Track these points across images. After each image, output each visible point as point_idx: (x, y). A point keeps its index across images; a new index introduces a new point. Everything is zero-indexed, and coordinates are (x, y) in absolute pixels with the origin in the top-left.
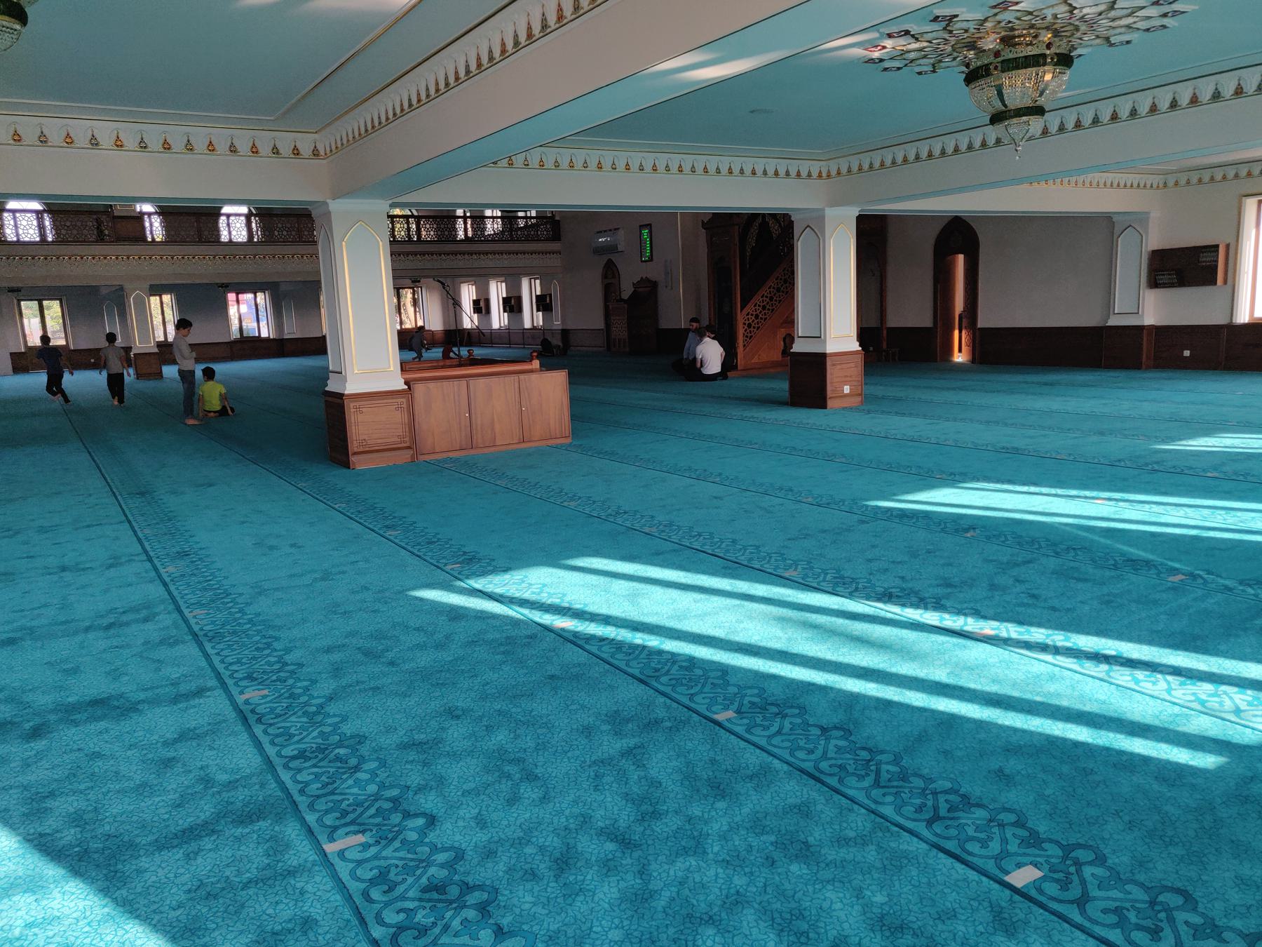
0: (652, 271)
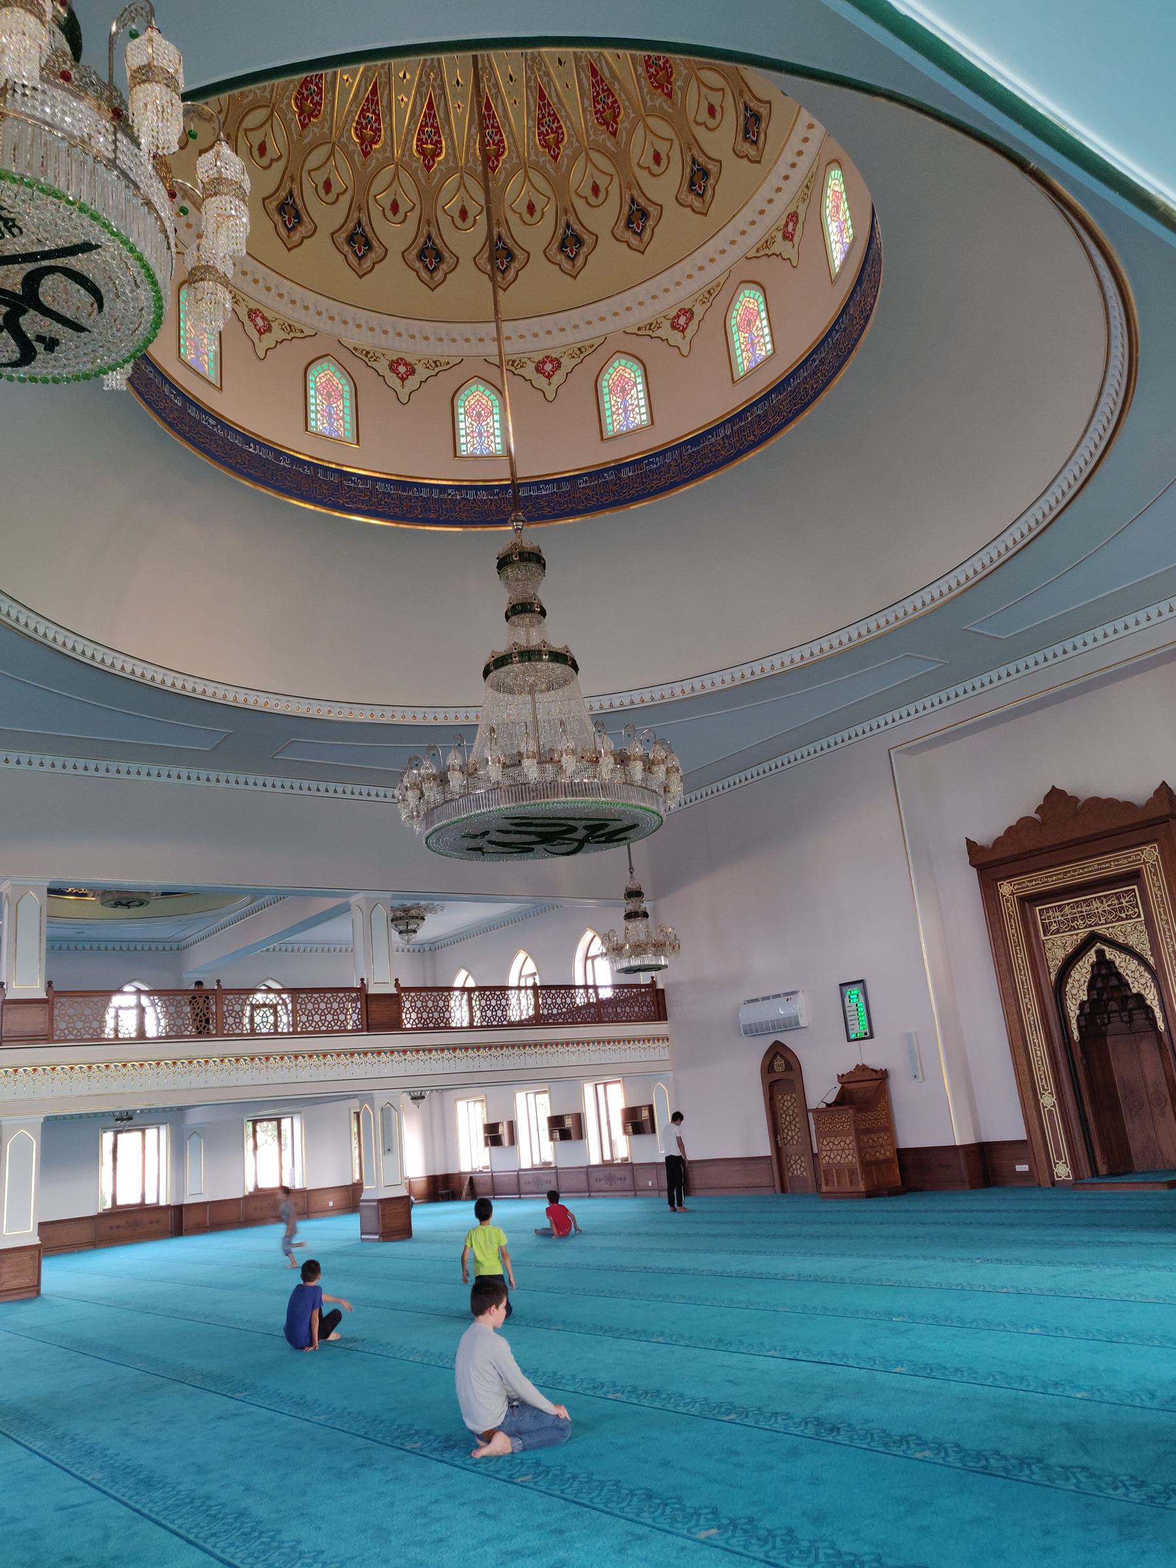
0: (873, 1055)
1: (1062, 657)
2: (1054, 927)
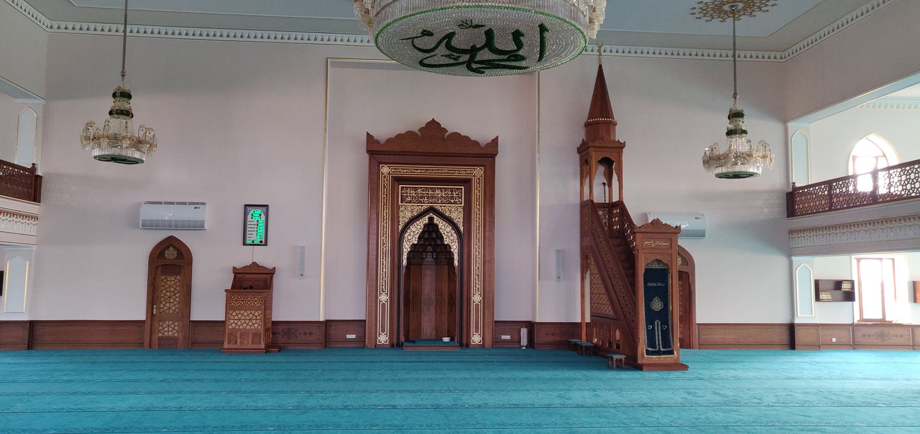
0: (263, 257)
1: (345, 43)
2: (409, 199)
